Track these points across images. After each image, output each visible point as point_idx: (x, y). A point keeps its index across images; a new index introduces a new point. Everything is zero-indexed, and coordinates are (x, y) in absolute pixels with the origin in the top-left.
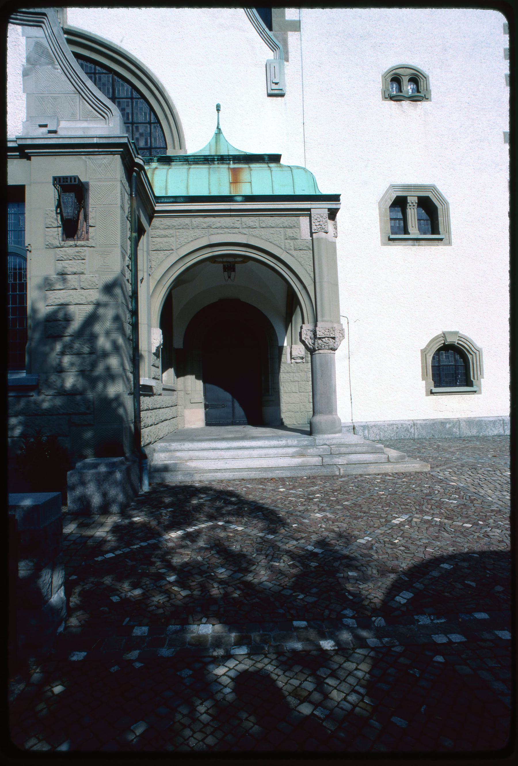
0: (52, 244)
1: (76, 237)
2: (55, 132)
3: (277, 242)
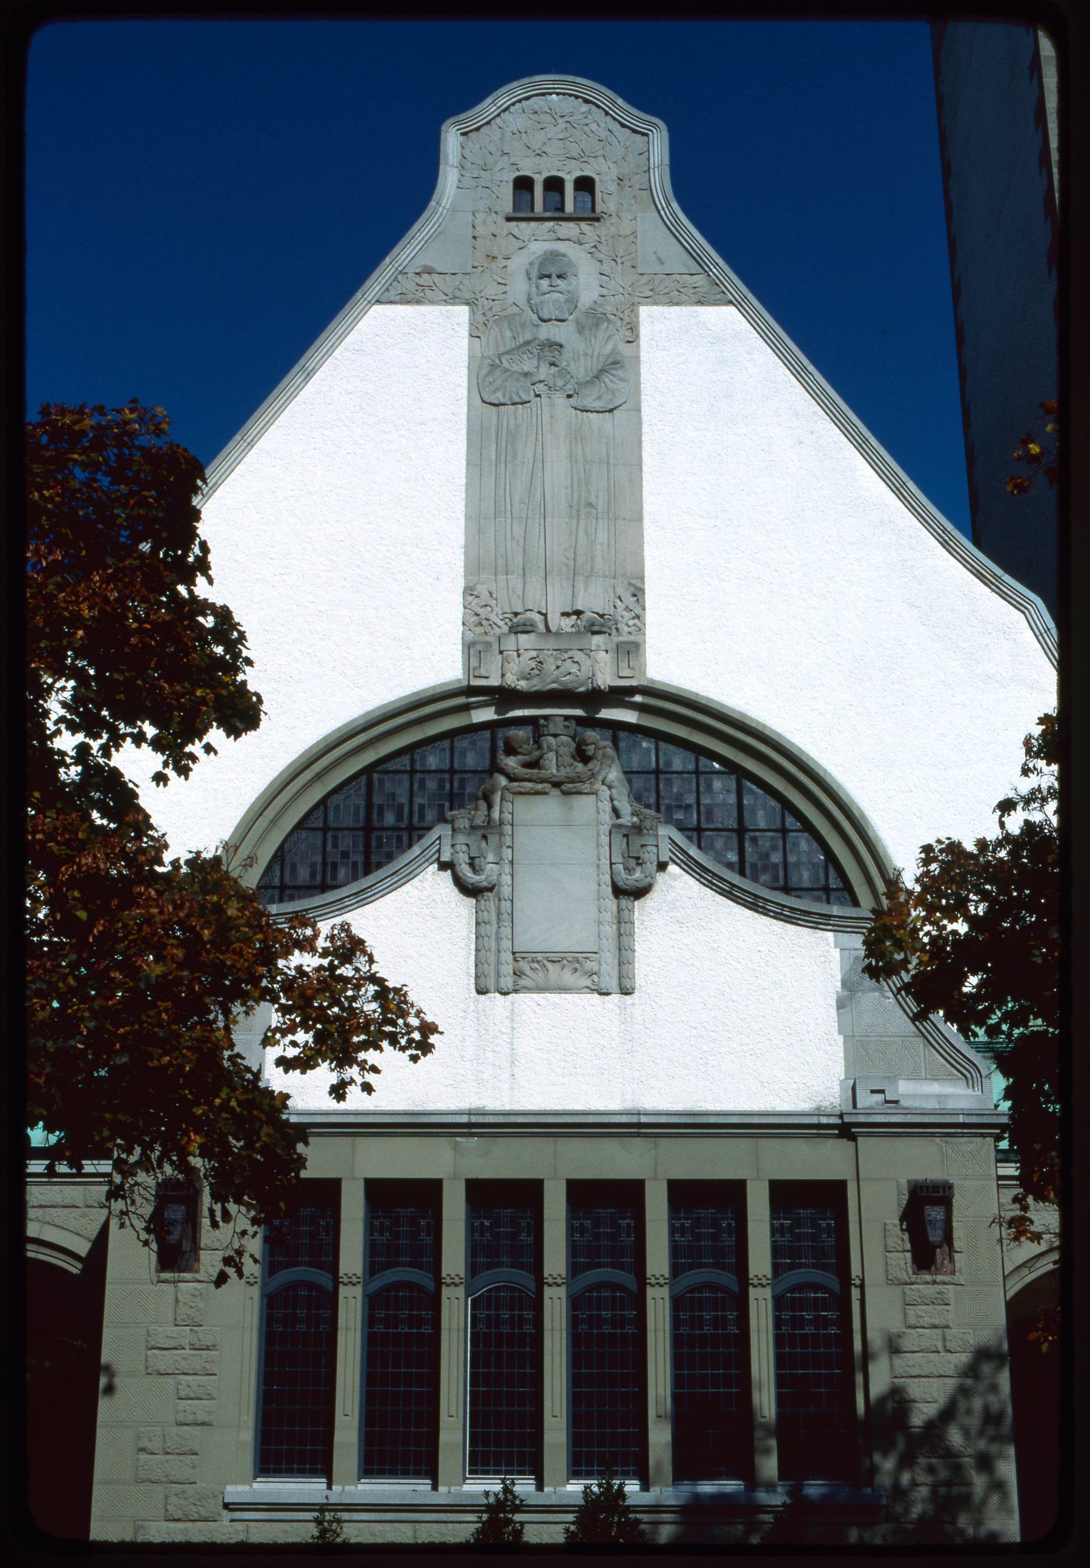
1: (933, 1269)
2: (896, 1102)
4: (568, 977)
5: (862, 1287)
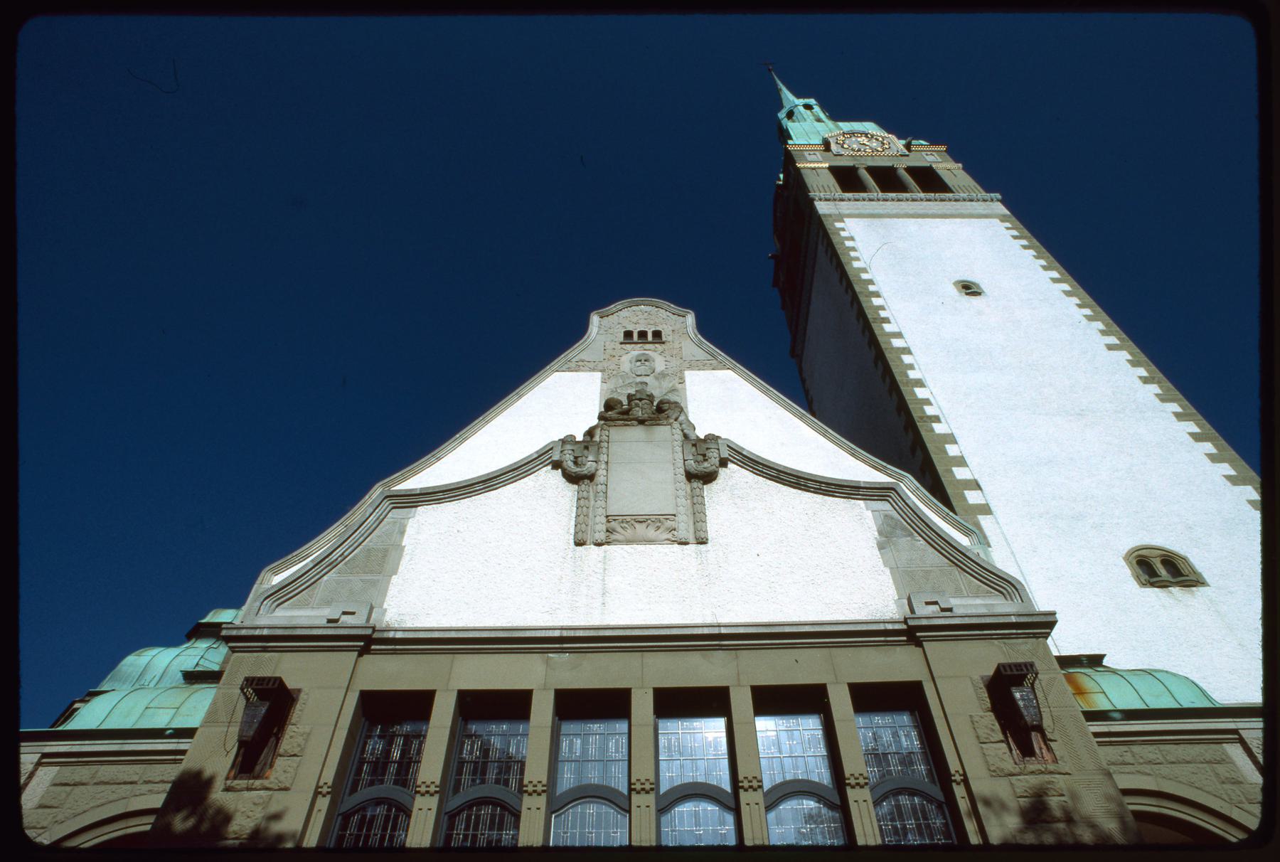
0: (1002, 770)
2: (950, 610)
3: (1210, 789)
4: (651, 533)
5: (966, 781)
